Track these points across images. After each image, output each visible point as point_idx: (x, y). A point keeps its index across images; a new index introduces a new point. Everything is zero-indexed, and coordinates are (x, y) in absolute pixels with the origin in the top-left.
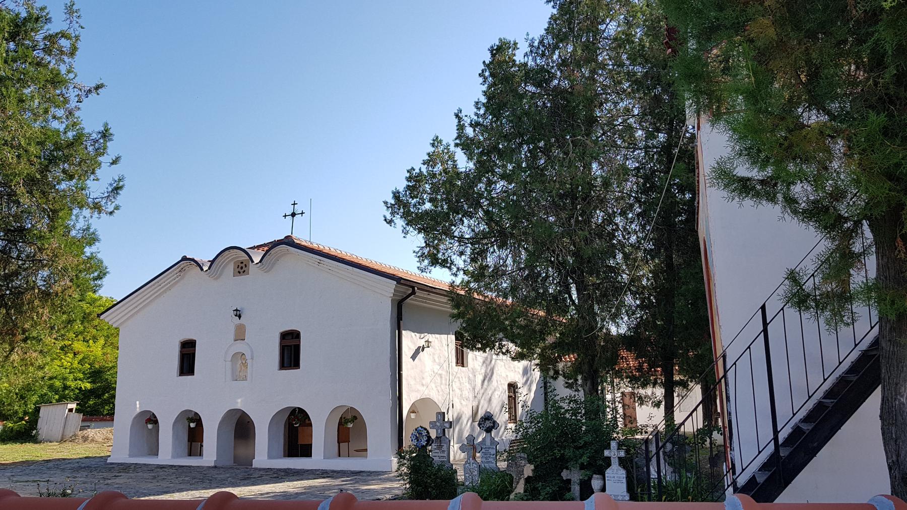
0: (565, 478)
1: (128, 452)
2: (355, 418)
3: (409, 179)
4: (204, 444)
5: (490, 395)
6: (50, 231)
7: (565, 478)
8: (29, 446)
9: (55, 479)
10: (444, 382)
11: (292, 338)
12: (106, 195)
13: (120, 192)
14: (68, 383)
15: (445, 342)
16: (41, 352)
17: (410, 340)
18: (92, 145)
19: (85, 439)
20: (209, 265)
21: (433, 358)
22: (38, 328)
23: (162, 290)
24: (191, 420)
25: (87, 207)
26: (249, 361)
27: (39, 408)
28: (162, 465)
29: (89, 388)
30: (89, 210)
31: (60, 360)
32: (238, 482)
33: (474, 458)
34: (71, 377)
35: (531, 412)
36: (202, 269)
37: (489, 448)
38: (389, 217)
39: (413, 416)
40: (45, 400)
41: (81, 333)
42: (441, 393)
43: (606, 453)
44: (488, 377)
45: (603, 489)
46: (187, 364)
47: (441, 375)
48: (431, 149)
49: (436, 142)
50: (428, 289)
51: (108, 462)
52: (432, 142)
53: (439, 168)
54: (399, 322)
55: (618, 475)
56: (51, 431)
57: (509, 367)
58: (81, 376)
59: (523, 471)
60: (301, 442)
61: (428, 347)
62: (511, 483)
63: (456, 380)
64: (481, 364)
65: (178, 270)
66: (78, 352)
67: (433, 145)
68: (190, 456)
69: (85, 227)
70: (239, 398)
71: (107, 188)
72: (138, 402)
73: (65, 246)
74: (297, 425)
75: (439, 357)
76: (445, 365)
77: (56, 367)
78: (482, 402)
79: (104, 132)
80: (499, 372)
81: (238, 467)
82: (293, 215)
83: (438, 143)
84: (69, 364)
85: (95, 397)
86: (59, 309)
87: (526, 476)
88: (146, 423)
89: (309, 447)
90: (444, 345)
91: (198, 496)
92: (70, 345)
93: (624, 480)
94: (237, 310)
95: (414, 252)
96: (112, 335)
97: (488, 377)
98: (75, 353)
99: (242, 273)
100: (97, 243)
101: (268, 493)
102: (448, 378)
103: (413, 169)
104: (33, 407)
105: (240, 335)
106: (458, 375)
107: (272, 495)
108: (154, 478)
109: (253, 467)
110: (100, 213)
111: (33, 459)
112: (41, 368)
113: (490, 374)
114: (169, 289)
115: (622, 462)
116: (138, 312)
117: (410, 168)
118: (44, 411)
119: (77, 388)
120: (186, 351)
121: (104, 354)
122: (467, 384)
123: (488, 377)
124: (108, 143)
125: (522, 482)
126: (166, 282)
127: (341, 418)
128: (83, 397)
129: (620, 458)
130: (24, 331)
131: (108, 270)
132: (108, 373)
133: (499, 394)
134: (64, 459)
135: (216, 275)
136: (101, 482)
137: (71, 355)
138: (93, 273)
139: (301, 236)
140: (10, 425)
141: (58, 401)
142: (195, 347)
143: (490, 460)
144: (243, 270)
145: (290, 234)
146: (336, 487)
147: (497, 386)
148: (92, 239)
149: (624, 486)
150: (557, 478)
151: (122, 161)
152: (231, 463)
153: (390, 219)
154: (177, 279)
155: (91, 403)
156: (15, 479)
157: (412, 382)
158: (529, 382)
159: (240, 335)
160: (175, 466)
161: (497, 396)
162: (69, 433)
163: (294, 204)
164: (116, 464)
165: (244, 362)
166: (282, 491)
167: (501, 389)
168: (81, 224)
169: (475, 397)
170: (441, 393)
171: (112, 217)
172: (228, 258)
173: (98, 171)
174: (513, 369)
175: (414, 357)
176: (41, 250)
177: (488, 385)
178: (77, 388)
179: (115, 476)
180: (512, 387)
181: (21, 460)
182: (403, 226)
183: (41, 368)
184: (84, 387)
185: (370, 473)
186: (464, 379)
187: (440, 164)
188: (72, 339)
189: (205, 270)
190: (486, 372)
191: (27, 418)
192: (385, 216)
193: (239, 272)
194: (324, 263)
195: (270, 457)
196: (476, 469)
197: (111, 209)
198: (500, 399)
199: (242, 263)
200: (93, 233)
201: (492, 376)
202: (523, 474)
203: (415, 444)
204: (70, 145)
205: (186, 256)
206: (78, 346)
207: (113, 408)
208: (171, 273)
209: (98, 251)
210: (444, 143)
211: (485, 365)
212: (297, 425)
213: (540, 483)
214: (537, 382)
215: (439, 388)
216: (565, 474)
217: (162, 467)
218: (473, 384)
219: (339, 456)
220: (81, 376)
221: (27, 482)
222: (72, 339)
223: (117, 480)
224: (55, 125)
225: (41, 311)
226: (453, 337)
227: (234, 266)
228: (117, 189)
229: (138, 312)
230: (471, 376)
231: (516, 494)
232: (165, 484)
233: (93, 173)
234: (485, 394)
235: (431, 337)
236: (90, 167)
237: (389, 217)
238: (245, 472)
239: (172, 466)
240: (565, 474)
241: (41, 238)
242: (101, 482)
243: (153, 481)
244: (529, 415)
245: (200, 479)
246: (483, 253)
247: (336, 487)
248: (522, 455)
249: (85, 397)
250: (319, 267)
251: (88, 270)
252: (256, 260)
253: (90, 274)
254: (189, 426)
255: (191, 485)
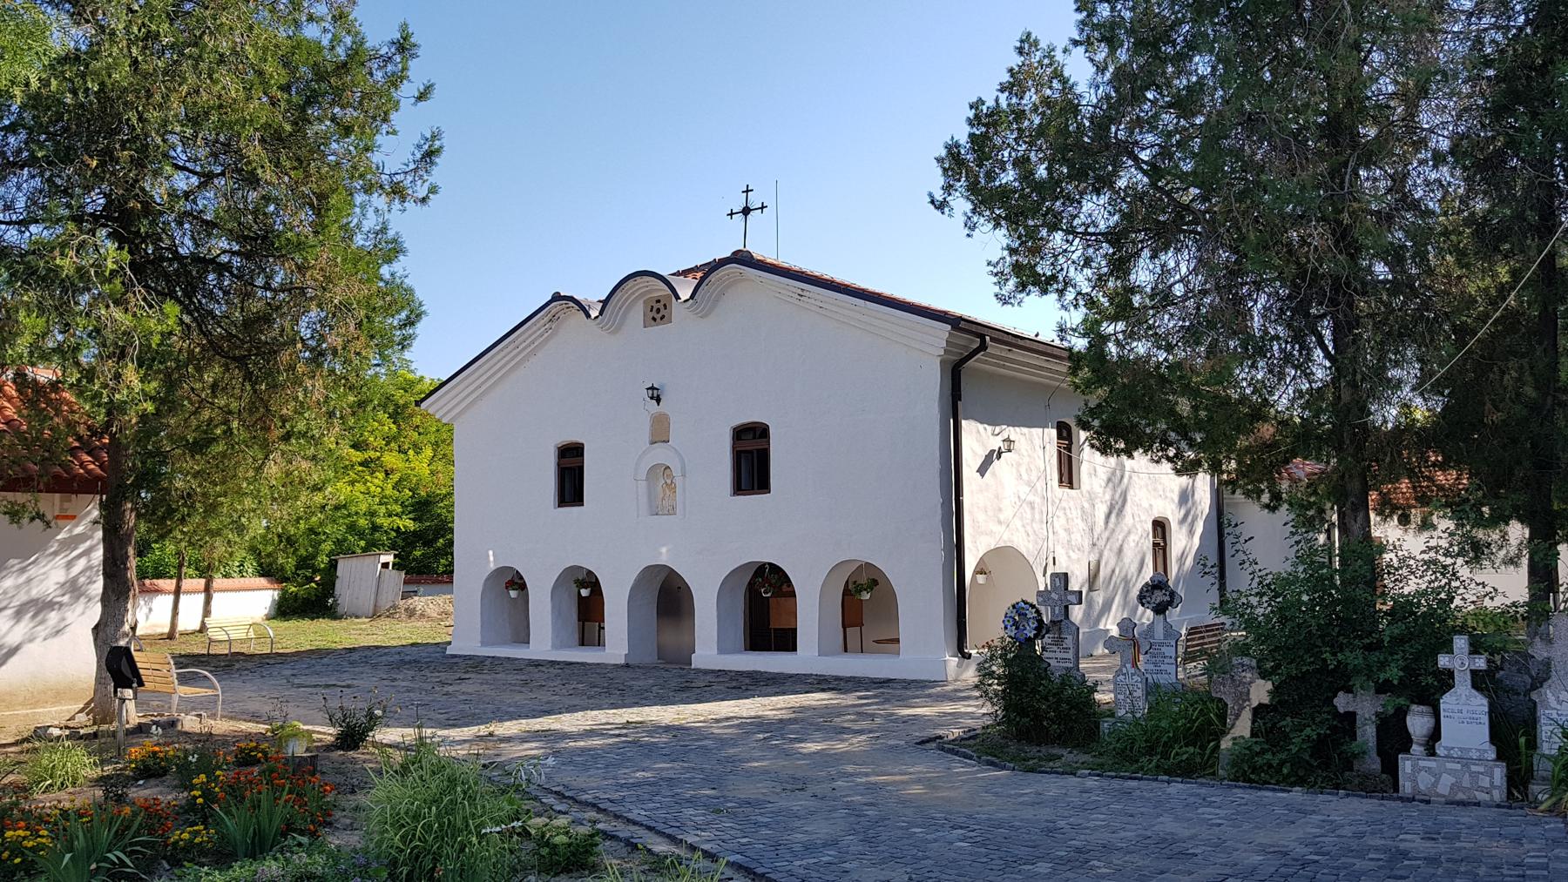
0: (1341, 710)
1: (479, 638)
2: (875, 582)
3: (975, 121)
4: (606, 625)
5: (1120, 542)
6: (316, 233)
7: (1341, 710)
8: (323, 624)
9: (362, 682)
10: (1037, 516)
11: (754, 438)
12: (412, 166)
13: (437, 160)
14: (379, 521)
15: (1038, 442)
16: (314, 458)
17: (976, 438)
18: (380, 68)
19: (411, 613)
20: (599, 308)
21: (1018, 471)
22: (306, 415)
23: (520, 357)
24: (581, 584)
25: (380, 191)
26: (678, 481)
27: (336, 561)
28: (537, 661)
29: (412, 529)
30: (384, 196)
31: (365, 484)
32: (671, 694)
33: (1135, 665)
34: (383, 510)
35: (1260, 574)
36: (588, 316)
37: (1162, 644)
38: (939, 196)
39: (981, 579)
40: (342, 548)
41: (395, 438)
42: (1032, 538)
43: (1443, 661)
44: (1117, 508)
45: (1435, 735)
46: (570, 487)
47: (1032, 505)
48: (1019, 60)
49: (1027, 44)
50: (1010, 339)
51: (447, 653)
52: (1018, 44)
53: (1031, 98)
54: (955, 405)
55: (1471, 708)
56: (357, 598)
57: (1155, 490)
58: (399, 509)
59: (1248, 693)
60: (775, 624)
61: (1009, 451)
62: (1222, 717)
63: (1060, 513)
64: (1103, 484)
65: (546, 319)
66: (392, 470)
67: (1020, 51)
68: (583, 645)
69: (378, 228)
70: (663, 545)
71: (413, 154)
72: (491, 553)
73: (344, 260)
74: (769, 595)
75: (1029, 470)
76: (1040, 485)
77: (358, 494)
78: (1106, 553)
79: (402, 41)
80: (1136, 499)
81: (668, 666)
82: (746, 211)
83: (1030, 48)
84: (379, 490)
85: (424, 544)
86: (343, 381)
87: (1255, 704)
88: (507, 588)
89: (793, 632)
90: (1037, 448)
91: (604, 721)
92: (379, 458)
93: (1485, 719)
94: (652, 388)
95: (989, 264)
96: (444, 441)
97: (1117, 507)
98: (386, 471)
99: (658, 320)
100: (401, 258)
101: (728, 719)
102: (1045, 509)
103: (981, 101)
104: (326, 560)
105: (660, 433)
106: (1064, 504)
107: (736, 722)
108: (525, 683)
109: (693, 667)
110: (403, 199)
111: (329, 645)
112: (317, 488)
113: (1120, 503)
114: (534, 353)
115: (1479, 681)
116: (483, 394)
117: (975, 100)
118: (345, 567)
119: (392, 529)
120: (570, 462)
121: (432, 473)
122: (1079, 521)
123: (1117, 507)
124: (410, 62)
125: (1246, 716)
126: (527, 342)
127: (847, 582)
128: (403, 544)
129: (1474, 673)
130: (284, 420)
131: (423, 308)
132: (442, 505)
133: (1137, 538)
134: (377, 647)
135: (613, 324)
136: (437, 688)
137: (381, 476)
138: (398, 312)
139: (759, 251)
140: (293, 589)
141: (365, 550)
142: (582, 455)
143: (1163, 667)
144: (660, 315)
145: (742, 248)
146: (851, 710)
147: (1134, 526)
148: (394, 250)
149: (1485, 731)
150: (1325, 709)
151: (436, 93)
152: (650, 658)
153: (941, 199)
154: (546, 335)
155: (418, 553)
156: (296, 681)
157: (981, 517)
158: (1190, 518)
159: (660, 433)
160: (558, 663)
161: (1132, 544)
162: (385, 603)
163: (747, 191)
164: (460, 656)
165: (669, 482)
166: (753, 714)
167: (1140, 530)
168: (371, 222)
169: (1094, 545)
170: (1032, 538)
171: (425, 208)
172: (633, 293)
173: (393, 116)
174: (1161, 493)
175: (982, 470)
176: (301, 269)
177: (1117, 523)
178: (392, 529)
179: (460, 679)
180: (1160, 526)
181: (309, 648)
182: (965, 214)
183: (317, 488)
184: (404, 527)
185: (908, 684)
186: (1074, 511)
187: (1033, 90)
188: (381, 448)
189: (593, 316)
190: (1112, 499)
191: (318, 578)
192: (931, 195)
193: (654, 319)
194: (811, 295)
195: (722, 650)
196: (1140, 685)
197: (422, 193)
198: (1139, 548)
199: (658, 301)
200: (395, 241)
201: (1123, 505)
202: (1249, 700)
203: (1013, 635)
204: (343, 67)
205: (558, 293)
206: (391, 459)
207: (451, 564)
208: (535, 324)
209: (406, 273)
210: (1043, 45)
211: (1110, 485)
212: (769, 595)
213: (1289, 719)
214: (1204, 517)
215: (1029, 528)
216: (1342, 702)
217: (537, 664)
218: (1089, 520)
219: (846, 651)
220: (399, 509)
221: (315, 686)
222: (381, 448)
223: (464, 687)
224: (311, 32)
225: (309, 383)
226: (1054, 432)
227: (645, 307)
228: (430, 156)
229: (483, 394)
230: (1086, 505)
231: (1234, 739)
232: (543, 696)
233: (385, 120)
234: (1111, 540)
235: (1014, 433)
236: (379, 109)
237: (939, 196)
238: (680, 676)
239: (553, 663)
240: (1342, 702)
241: (300, 246)
242: (437, 688)
243: (523, 689)
244: (1257, 580)
245: (603, 688)
246: (1121, 266)
247: (851, 710)
248: (1246, 660)
249: (408, 544)
250: (801, 304)
251: (389, 310)
252: (685, 294)
253: (393, 316)
254: (579, 593)
255: (588, 698)
